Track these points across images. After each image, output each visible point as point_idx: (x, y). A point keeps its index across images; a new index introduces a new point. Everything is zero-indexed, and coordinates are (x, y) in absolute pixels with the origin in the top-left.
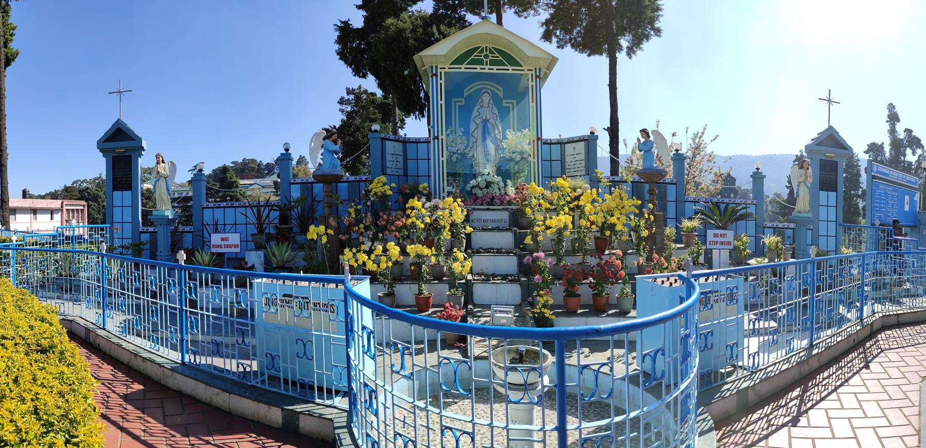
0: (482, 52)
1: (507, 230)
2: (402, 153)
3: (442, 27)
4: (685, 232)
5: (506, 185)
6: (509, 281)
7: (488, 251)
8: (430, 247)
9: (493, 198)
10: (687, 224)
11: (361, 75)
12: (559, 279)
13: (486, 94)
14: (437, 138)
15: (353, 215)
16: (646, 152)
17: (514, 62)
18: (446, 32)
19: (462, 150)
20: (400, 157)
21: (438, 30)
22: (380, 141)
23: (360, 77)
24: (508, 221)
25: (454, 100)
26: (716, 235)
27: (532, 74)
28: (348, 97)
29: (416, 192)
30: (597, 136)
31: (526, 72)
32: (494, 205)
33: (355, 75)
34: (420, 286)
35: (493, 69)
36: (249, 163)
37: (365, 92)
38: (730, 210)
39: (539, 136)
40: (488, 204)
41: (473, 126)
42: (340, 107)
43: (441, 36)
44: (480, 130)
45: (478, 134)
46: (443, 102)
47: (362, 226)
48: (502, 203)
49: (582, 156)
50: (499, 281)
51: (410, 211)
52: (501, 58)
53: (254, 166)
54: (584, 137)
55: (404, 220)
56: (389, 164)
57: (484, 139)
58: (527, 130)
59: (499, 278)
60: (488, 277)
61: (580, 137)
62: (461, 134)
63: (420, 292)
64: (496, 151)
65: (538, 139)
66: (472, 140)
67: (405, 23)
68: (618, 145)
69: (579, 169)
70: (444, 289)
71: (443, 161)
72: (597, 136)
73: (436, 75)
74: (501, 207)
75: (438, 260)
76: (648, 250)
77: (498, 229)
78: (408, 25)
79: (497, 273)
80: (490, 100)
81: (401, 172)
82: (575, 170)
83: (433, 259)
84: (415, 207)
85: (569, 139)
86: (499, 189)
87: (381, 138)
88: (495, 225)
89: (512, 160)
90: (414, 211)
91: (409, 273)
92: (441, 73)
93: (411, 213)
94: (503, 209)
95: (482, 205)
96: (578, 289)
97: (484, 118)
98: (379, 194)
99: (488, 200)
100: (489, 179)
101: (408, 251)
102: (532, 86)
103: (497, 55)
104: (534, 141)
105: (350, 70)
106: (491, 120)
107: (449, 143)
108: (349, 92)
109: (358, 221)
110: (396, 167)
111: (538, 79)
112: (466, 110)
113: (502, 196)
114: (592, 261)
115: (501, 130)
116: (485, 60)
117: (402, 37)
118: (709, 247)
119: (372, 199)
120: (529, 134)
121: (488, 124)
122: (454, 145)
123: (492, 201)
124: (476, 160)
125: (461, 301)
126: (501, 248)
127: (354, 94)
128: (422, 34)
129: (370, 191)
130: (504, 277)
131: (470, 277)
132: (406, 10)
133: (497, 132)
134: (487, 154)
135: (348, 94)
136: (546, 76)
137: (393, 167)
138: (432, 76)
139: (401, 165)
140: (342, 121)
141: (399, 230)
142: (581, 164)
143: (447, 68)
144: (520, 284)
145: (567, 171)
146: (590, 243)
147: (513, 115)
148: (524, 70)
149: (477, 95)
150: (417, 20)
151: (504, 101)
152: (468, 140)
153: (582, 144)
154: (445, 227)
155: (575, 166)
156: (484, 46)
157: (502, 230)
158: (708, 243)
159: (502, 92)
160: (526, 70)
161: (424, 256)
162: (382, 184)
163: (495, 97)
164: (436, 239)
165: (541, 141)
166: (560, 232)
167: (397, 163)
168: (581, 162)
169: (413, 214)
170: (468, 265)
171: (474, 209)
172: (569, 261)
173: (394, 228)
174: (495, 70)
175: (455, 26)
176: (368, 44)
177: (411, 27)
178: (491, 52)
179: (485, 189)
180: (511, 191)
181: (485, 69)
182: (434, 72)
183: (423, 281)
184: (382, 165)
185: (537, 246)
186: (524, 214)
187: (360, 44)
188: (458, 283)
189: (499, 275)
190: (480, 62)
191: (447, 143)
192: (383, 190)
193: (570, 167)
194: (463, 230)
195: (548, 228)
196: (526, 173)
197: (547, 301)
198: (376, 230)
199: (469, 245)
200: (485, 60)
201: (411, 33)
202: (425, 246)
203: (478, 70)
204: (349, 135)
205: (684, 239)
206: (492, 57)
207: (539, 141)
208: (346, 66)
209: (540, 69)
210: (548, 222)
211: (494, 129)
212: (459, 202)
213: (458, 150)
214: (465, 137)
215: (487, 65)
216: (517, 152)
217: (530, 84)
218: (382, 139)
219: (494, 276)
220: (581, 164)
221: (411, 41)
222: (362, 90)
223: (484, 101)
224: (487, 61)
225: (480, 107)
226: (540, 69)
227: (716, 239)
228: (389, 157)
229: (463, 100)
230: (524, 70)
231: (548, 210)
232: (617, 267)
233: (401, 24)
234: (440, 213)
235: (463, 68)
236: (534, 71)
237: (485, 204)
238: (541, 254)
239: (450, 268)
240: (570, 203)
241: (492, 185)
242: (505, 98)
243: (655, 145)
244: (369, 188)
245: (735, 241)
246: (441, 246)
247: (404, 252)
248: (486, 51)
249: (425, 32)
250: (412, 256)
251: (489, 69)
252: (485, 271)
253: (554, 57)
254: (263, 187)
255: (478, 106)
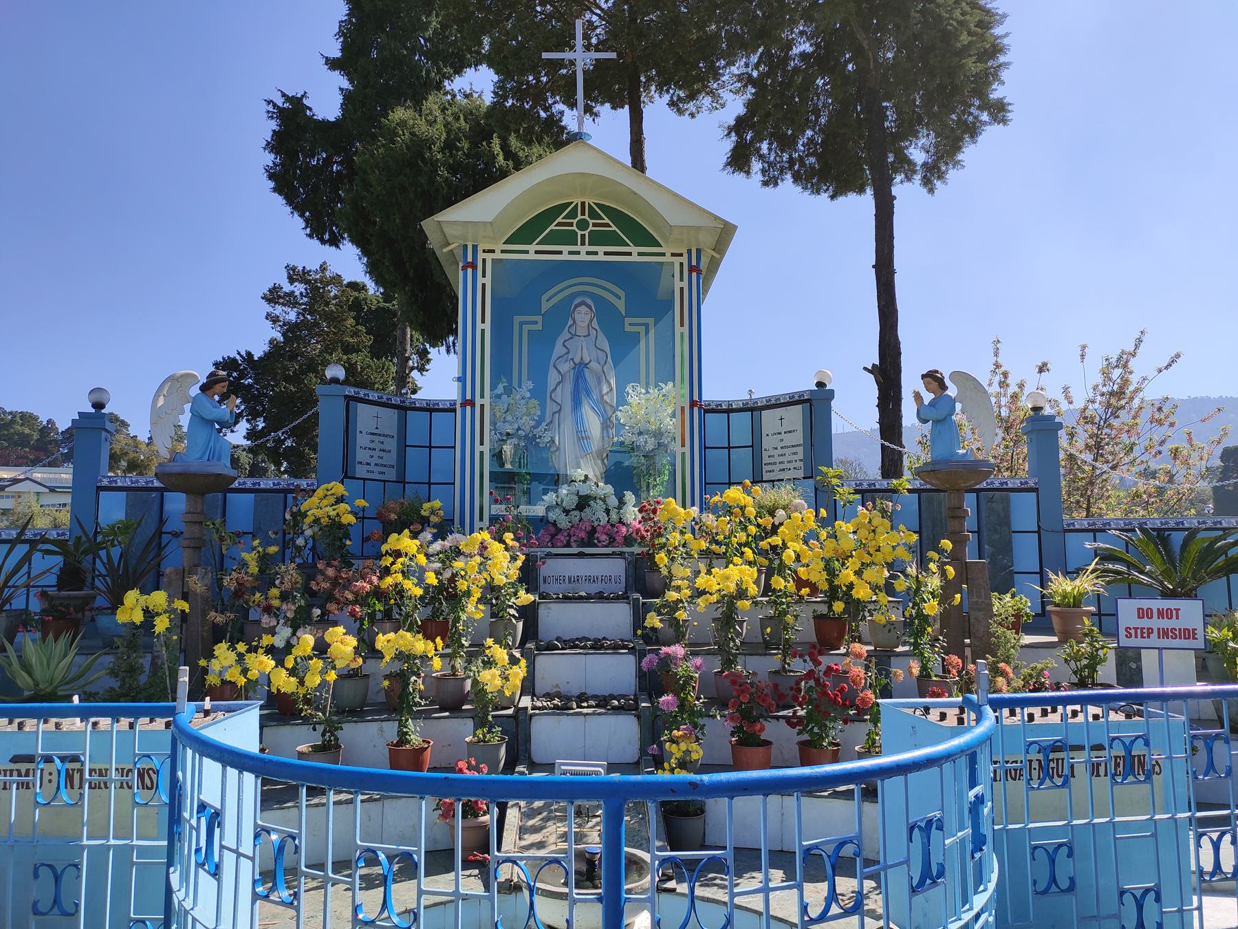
0: (573, 214)
1: (617, 598)
2: (394, 433)
3: (514, 142)
4: (1057, 605)
5: (622, 503)
6: (614, 708)
7: (571, 644)
8: (429, 637)
9: (593, 530)
10: (1061, 585)
11: (327, 237)
12: (723, 705)
13: (583, 309)
14: (472, 403)
15: (254, 568)
16: (937, 422)
17: (643, 237)
18: (521, 154)
19: (527, 428)
20: (389, 439)
21: (505, 147)
22: (343, 403)
23: (323, 242)
24: (623, 579)
25: (517, 319)
26: (1141, 614)
27: (681, 264)
28: (292, 288)
29: (411, 521)
30: (832, 391)
31: (668, 258)
32: (595, 546)
33: (310, 236)
34: (402, 725)
35: (596, 253)
36: (13, 421)
37: (337, 279)
38: (1194, 549)
39: (696, 398)
40: (582, 543)
41: (553, 377)
42: (270, 310)
43: (511, 163)
44: (568, 387)
45: (564, 394)
46: (487, 326)
47: (274, 592)
48: (612, 541)
49: (798, 437)
50: (590, 711)
51: (391, 559)
52: (614, 228)
53: (27, 431)
54: (801, 394)
55: (375, 579)
56: (361, 455)
57: (577, 403)
58: (670, 384)
59: (593, 703)
60: (564, 703)
61: (792, 395)
62: (528, 395)
63: (403, 738)
64: (603, 429)
65: (693, 404)
66: (551, 407)
67: (432, 123)
68: (900, 406)
69: (791, 466)
70: (464, 731)
71: (482, 453)
72: (832, 391)
73: (473, 266)
74: (609, 550)
75: (453, 667)
76: (943, 647)
77: (600, 597)
78: (438, 132)
79: (590, 692)
80: (591, 321)
81: (391, 474)
82: (782, 466)
83: (437, 663)
84: (403, 551)
85: (769, 399)
86: (608, 511)
87: (346, 397)
88: (594, 589)
89: (633, 448)
90: (400, 560)
91: (382, 698)
92: (484, 261)
93: (393, 563)
94: (614, 553)
95: (568, 545)
96: (762, 729)
97: (577, 360)
98: (325, 521)
99: (583, 535)
100: (584, 490)
101: (379, 646)
102: (682, 289)
103: (607, 221)
104: (683, 409)
105: (299, 222)
106: (594, 365)
107: (498, 414)
108: (295, 275)
109: (265, 580)
110: (380, 461)
111: (694, 274)
112: (543, 341)
113: (613, 526)
114: (799, 666)
115: (614, 385)
116: (580, 233)
117: (423, 159)
118: (1125, 642)
119: (309, 532)
120: (673, 393)
121: (587, 373)
122: (509, 418)
123: (590, 538)
124: (558, 449)
125: (498, 756)
126: (604, 638)
127: (307, 282)
128: (468, 156)
129: (305, 515)
130: (603, 702)
131: (526, 702)
132: (439, 86)
133: (605, 389)
134: (581, 436)
135: (291, 280)
136: (714, 265)
137: (373, 461)
138: (465, 268)
139: (391, 458)
140: (271, 342)
141: (361, 600)
142: (795, 453)
143: (498, 251)
144: (638, 717)
145: (765, 468)
146: (802, 627)
147: (647, 348)
148: (663, 254)
149: (563, 312)
150: (457, 119)
151: (628, 320)
152: (543, 407)
153: (796, 412)
154: (468, 594)
155: (781, 459)
156: (577, 201)
157: (607, 598)
158: (1122, 633)
159: (623, 298)
160: (668, 254)
161: (415, 657)
162: (332, 500)
163: (604, 312)
164: (452, 616)
165: (700, 408)
166: (729, 602)
167: (382, 454)
168: (794, 450)
169: (398, 566)
170: (516, 675)
171: (549, 555)
172: (758, 667)
173: (350, 596)
174: (601, 254)
175: (540, 142)
176: (348, 163)
177: (444, 136)
178: (593, 215)
179: (576, 513)
180: (631, 513)
181: (578, 253)
182: (470, 259)
183: (410, 712)
184: (346, 457)
185: (677, 632)
186: (655, 567)
187: (328, 162)
188: (493, 717)
189: (594, 697)
190: (570, 239)
191: (493, 415)
192: (333, 513)
193: (772, 460)
194: (513, 600)
195: (701, 593)
196: (666, 478)
197: (688, 752)
198: (306, 601)
199: (531, 632)
200: (580, 233)
201: (442, 150)
202: (420, 636)
203: (565, 257)
204: (288, 379)
205: (1056, 621)
206: (594, 225)
207: (696, 410)
208: (289, 209)
209: (699, 251)
210: (701, 582)
211: (599, 383)
212: (508, 541)
213: (519, 429)
214: (535, 402)
215: (583, 244)
216: (647, 432)
217: (678, 284)
218: (349, 398)
219: (582, 698)
220: (795, 453)
221: (443, 172)
222: (328, 274)
223: (578, 322)
224: (583, 236)
225: (569, 336)
226: (699, 251)
227: (1145, 623)
228: (362, 440)
229: (539, 318)
230: (663, 254)
231: (706, 554)
232: (853, 682)
233: (422, 127)
234: (459, 564)
235: (531, 252)
236: (686, 256)
237: (573, 544)
238: (678, 650)
239: (475, 682)
240: (757, 538)
241: (592, 503)
242: (629, 314)
243: (958, 406)
244: (303, 509)
245: (1210, 629)
246: (461, 635)
247: (367, 648)
248: (583, 214)
249: (474, 153)
250: (387, 658)
251: (588, 253)
252: (564, 689)
253: (726, 223)
254: (52, 490)
255: (565, 335)
